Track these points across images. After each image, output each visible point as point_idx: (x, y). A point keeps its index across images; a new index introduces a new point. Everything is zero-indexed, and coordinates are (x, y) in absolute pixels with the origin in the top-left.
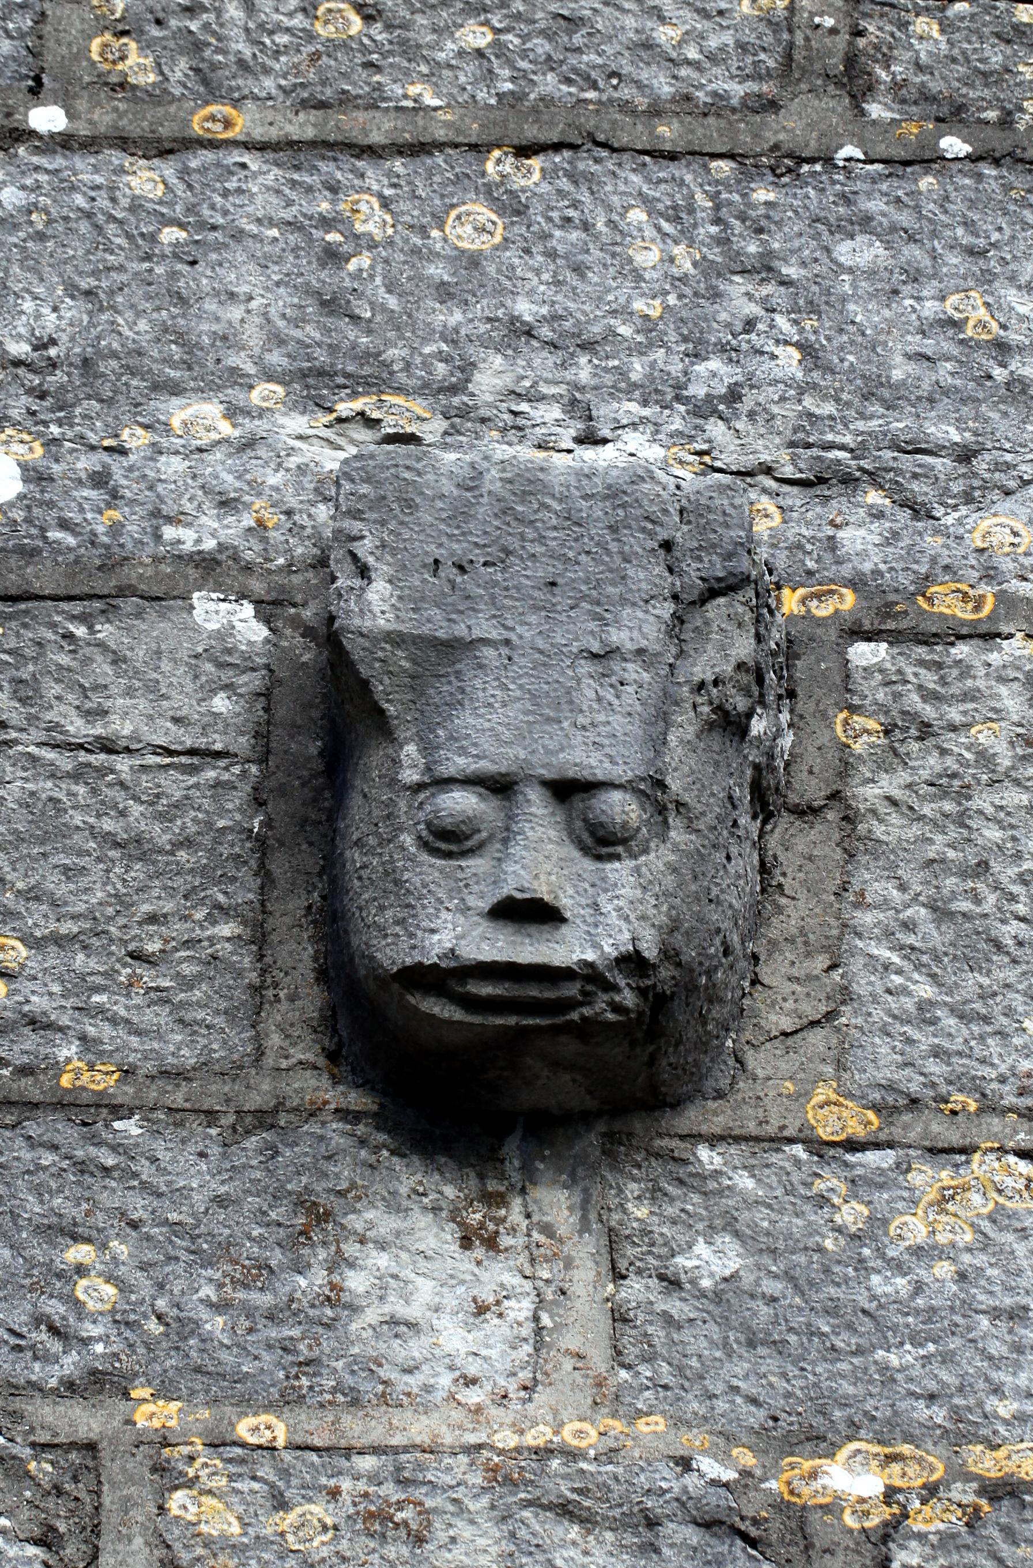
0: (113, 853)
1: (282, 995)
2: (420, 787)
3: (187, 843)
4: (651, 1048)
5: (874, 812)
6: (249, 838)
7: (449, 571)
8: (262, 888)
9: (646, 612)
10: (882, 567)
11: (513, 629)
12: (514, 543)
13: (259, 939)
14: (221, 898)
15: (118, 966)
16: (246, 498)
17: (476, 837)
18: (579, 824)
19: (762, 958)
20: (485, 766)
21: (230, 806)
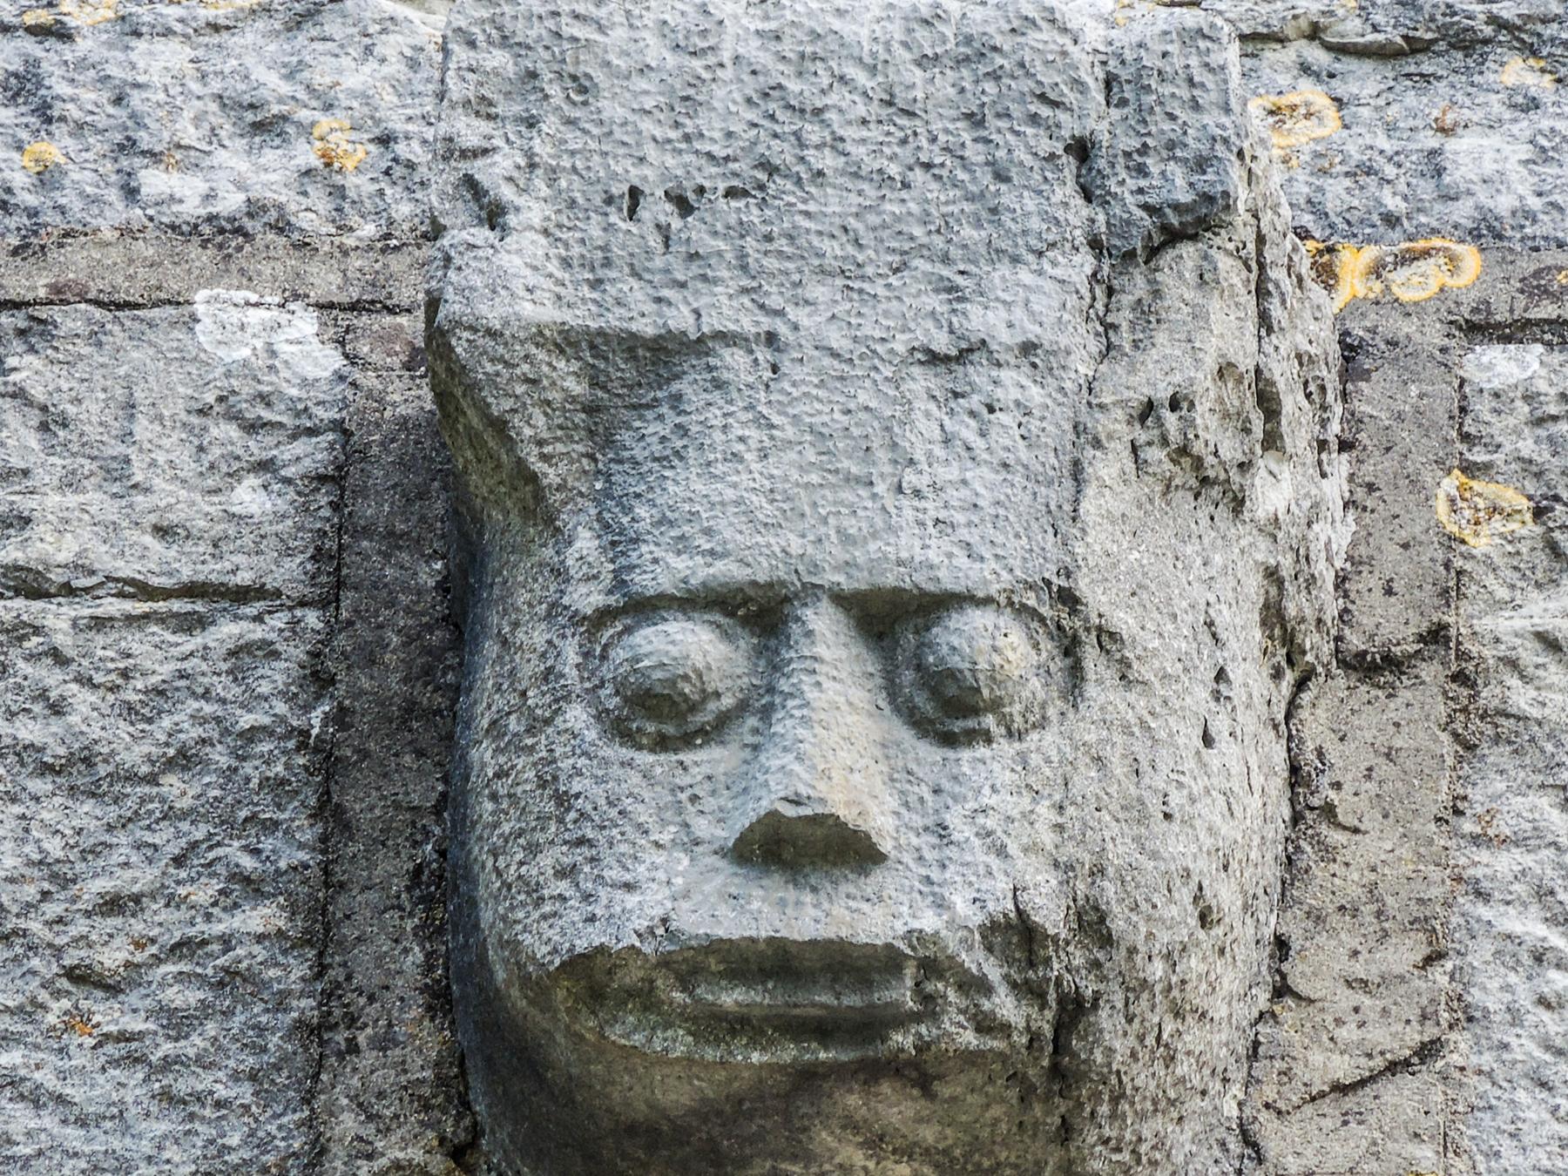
0: (39, 786)
1: (362, 1039)
2: (604, 616)
3: (184, 760)
4: (1063, 1106)
5: (1513, 664)
6: (302, 746)
7: (657, 209)
8: (324, 839)
9: (1040, 273)
10: (1535, 203)
11: (780, 313)
12: (781, 152)
13: (319, 933)
14: (248, 863)
15: (43, 996)
16: (303, 115)
17: (712, 706)
18: (908, 676)
19: (1295, 946)
20: (728, 571)
21: (265, 688)
